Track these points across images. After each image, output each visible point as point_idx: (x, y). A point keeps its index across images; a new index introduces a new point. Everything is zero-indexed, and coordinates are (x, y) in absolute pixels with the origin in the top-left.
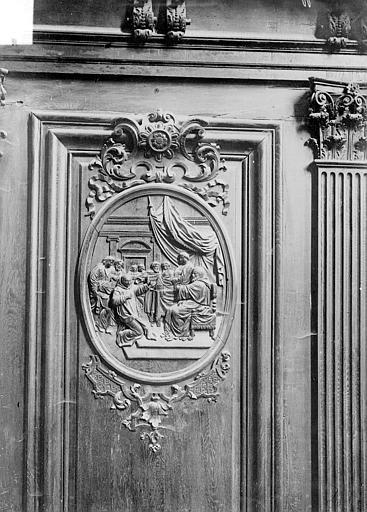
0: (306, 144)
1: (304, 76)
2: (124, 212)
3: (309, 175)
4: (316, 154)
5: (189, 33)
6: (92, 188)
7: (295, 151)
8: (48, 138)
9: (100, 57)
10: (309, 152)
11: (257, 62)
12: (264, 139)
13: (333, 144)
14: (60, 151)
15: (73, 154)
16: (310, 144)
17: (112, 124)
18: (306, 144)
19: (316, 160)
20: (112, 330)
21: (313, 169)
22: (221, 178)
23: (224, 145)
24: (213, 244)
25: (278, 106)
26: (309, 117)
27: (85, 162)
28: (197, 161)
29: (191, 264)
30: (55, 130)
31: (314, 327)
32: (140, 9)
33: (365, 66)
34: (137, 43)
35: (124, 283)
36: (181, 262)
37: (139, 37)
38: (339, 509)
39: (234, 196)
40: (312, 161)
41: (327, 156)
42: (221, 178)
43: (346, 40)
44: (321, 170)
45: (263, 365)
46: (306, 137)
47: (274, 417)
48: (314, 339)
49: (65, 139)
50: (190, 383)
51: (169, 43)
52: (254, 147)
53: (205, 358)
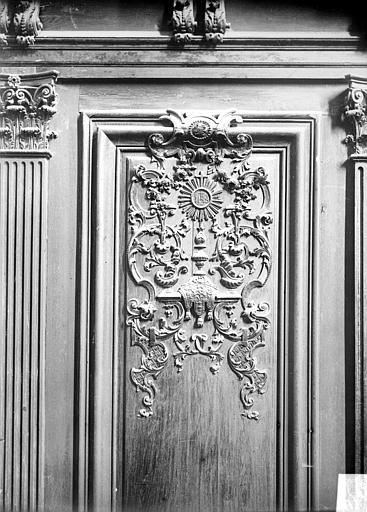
0: (344, 142)
1: (340, 74)
5: (230, 34)
7: (332, 148)
8: (95, 136)
9: (142, 61)
10: (344, 149)
11: (296, 61)
12: (301, 130)
14: (107, 148)
15: (122, 151)
18: (344, 142)
19: (352, 155)
21: (349, 165)
25: (314, 103)
26: (341, 115)
30: (104, 127)
32: (212, 15)
33: (365, 62)
34: (175, 46)
37: (211, 40)
40: (346, 158)
43: (190, 35)
44: (357, 165)
45: (300, 501)
46: (342, 135)
47: (311, 473)
49: (112, 137)
51: (210, 45)
52: (292, 139)
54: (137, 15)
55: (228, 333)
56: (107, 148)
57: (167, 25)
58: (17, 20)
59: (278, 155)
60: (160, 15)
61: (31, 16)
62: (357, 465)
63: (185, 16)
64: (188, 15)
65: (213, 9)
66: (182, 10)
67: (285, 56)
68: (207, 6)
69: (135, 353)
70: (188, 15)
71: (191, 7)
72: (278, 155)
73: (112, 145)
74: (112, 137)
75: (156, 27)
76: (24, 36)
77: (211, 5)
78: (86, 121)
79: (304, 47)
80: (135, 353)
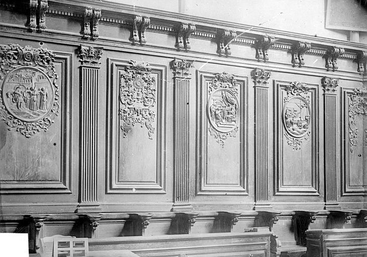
2: (216, 94)
3: (173, 80)
4: (324, 92)
5: (146, 44)
6: (210, 88)
12: (68, 57)
13: (259, 82)
16: (324, 90)
17: (215, 74)
20: (215, 120)
22: (236, 88)
23: (238, 80)
24: (235, 103)
27: (208, 82)
28: (232, 84)
29: (231, 106)
31: (255, 122)
35: (218, 110)
36: (229, 106)
38: (2, 192)
39: (239, 92)
41: (258, 85)
42: (236, 88)
44: (83, 68)
48: (255, 125)
50: (230, 133)
53: (234, 127)
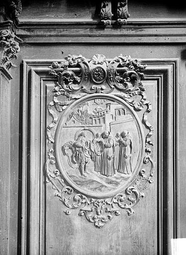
12: (169, 68)
15: (43, 80)
30: (33, 68)
33: (185, 32)
34: (101, 26)
49: (37, 72)
51: (117, 26)
52: (165, 72)
54: (142, 8)
55: (53, 157)
56: (35, 78)
57: (97, 15)
58: (103, 11)
59: (156, 81)
60: (93, 9)
61: (125, 9)
62: (179, 235)
63: (107, 11)
64: (108, 10)
65: (104, 7)
66: (105, 7)
67: (73, 31)
68: (119, 5)
69: (110, 199)
70: (108, 10)
71: (127, 6)
72: (156, 81)
73: (38, 77)
74: (37, 72)
75: (91, 15)
76: (105, 20)
77: (121, 4)
78: (25, 64)
79: (161, 26)
80: (110, 199)
